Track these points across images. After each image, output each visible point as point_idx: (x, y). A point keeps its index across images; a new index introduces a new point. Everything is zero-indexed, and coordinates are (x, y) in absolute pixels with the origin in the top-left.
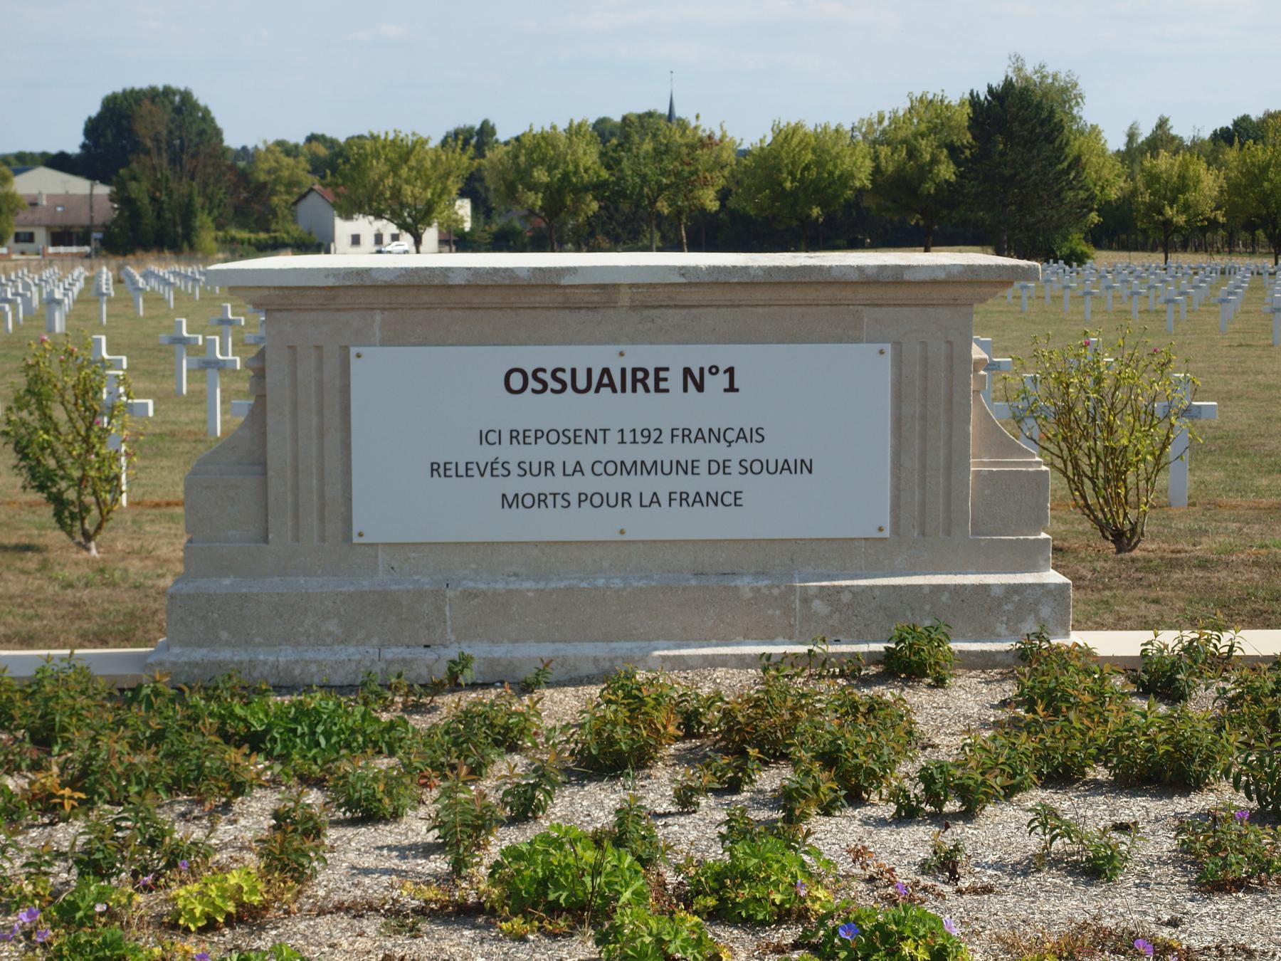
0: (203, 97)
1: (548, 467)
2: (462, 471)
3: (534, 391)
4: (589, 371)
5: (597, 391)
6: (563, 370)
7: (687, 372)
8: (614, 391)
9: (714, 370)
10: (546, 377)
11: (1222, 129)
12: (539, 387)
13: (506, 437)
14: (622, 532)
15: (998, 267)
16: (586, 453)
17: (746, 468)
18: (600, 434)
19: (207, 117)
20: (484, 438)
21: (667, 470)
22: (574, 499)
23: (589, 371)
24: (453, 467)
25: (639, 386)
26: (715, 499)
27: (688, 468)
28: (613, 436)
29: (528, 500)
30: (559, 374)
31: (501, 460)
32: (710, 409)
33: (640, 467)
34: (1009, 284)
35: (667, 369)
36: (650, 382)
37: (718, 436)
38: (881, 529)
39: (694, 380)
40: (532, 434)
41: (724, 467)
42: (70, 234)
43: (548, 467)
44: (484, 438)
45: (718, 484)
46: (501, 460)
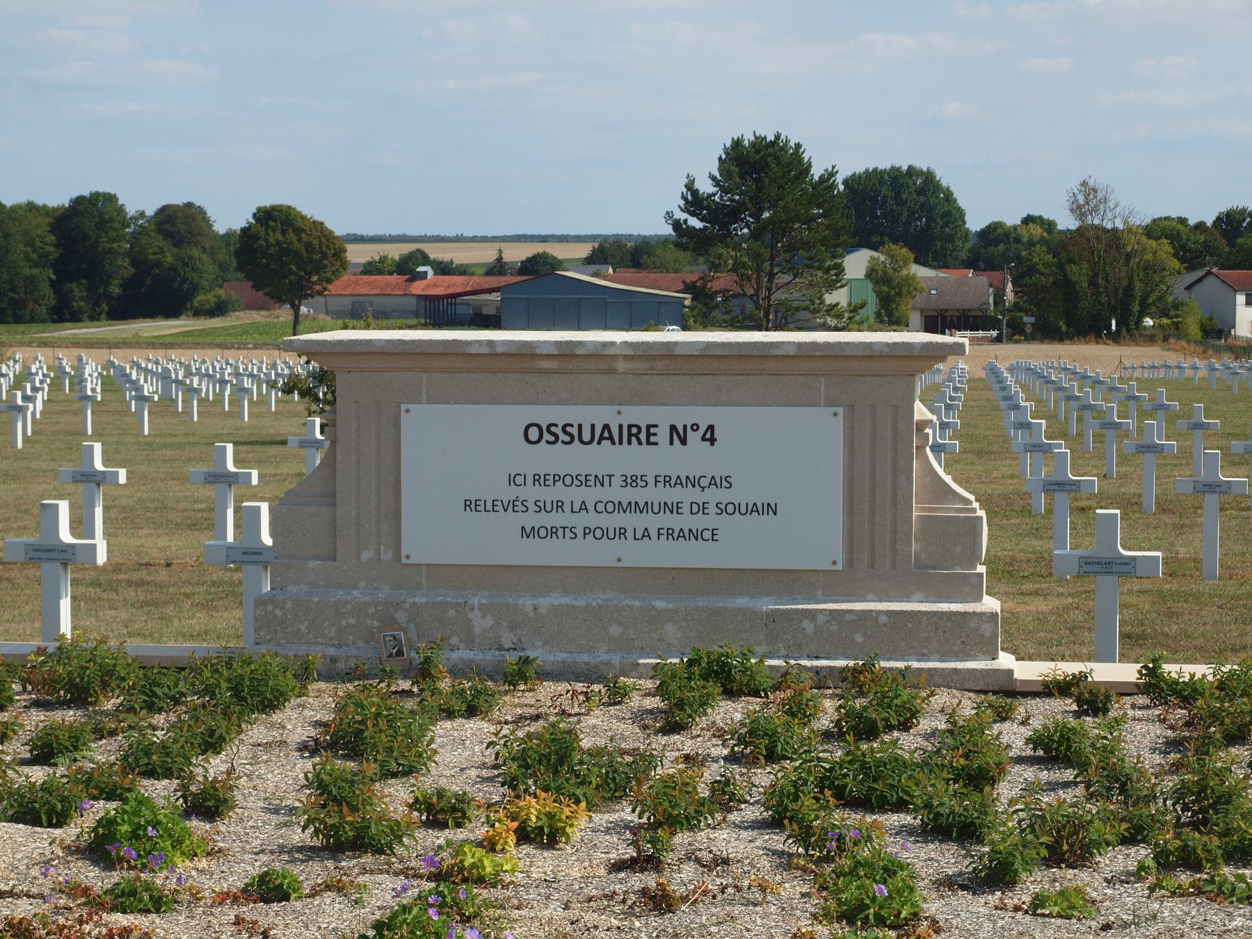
0: (946, 178)
1: (559, 505)
2: (489, 507)
3: (548, 442)
4: (593, 426)
5: (599, 443)
6: (572, 426)
7: (673, 428)
8: (613, 443)
9: (695, 427)
10: (558, 431)
11: (875, 170)
12: (552, 439)
13: (530, 480)
14: (619, 560)
15: (929, 344)
16: (591, 495)
17: (722, 510)
18: (606, 479)
19: (949, 197)
20: (512, 480)
21: (656, 510)
22: (580, 533)
23: (593, 426)
24: (482, 503)
25: (634, 439)
26: (696, 535)
27: (674, 509)
28: (617, 481)
29: (543, 532)
30: (568, 429)
31: (521, 499)
32: (694, 458)
33: (634, 507)
34: (942, 359)
35: (656, 426)
36: (643, 436)
37: (693, 482)
38: (834, 563)
39: (678, 435)
40: (551, 478)
41: (703, 508)
42: (967, 317)
43: (559, 505)
44: (512, 480)
45: (698, 522)
46: (521, 499)
